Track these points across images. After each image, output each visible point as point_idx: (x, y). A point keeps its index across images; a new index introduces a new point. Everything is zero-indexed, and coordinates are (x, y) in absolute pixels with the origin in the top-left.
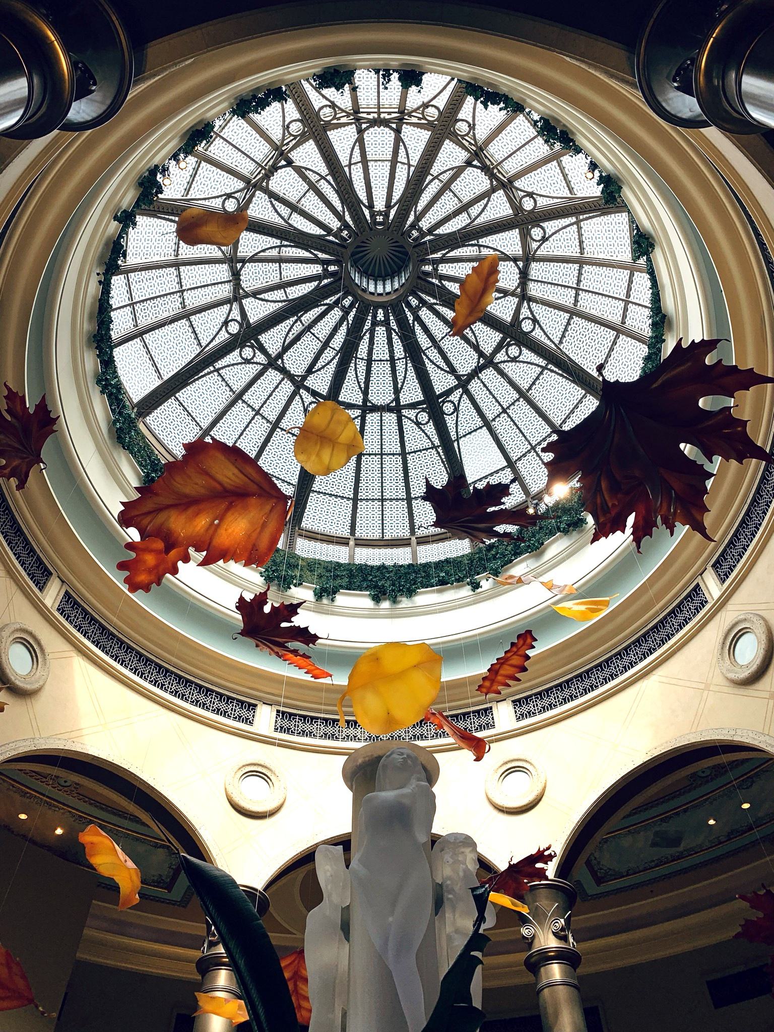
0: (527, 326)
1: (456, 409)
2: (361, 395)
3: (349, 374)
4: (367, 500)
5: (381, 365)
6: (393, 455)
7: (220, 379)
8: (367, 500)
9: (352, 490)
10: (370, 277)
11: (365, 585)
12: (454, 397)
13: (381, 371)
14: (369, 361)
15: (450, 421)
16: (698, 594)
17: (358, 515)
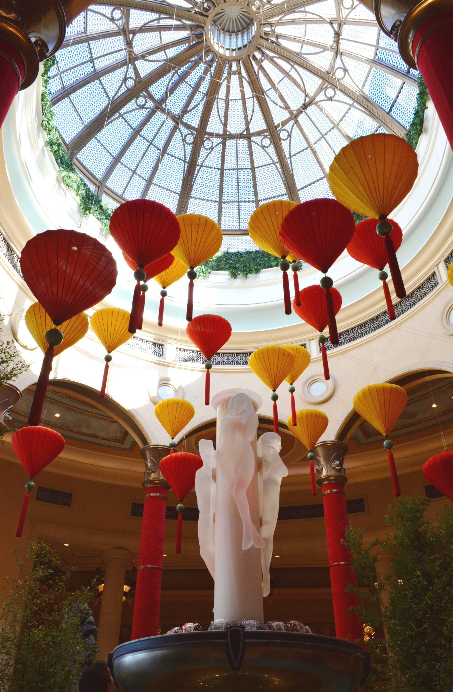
0: (339, 74)
1: (290, 136)
2: (222, 126)
3: (213, 111)
4: (228, 202)
5: (236, 103)
6: (246, 169)
7: (126, 124)
8: (228, 202)
9: (218, 195)
10: (227, 33)
11: (227, 266)
12: (288, 127)
13: (227, 213)
14: (227, 101)
15: (285, 145)
16: (434, 278)
17: (222, 213)
